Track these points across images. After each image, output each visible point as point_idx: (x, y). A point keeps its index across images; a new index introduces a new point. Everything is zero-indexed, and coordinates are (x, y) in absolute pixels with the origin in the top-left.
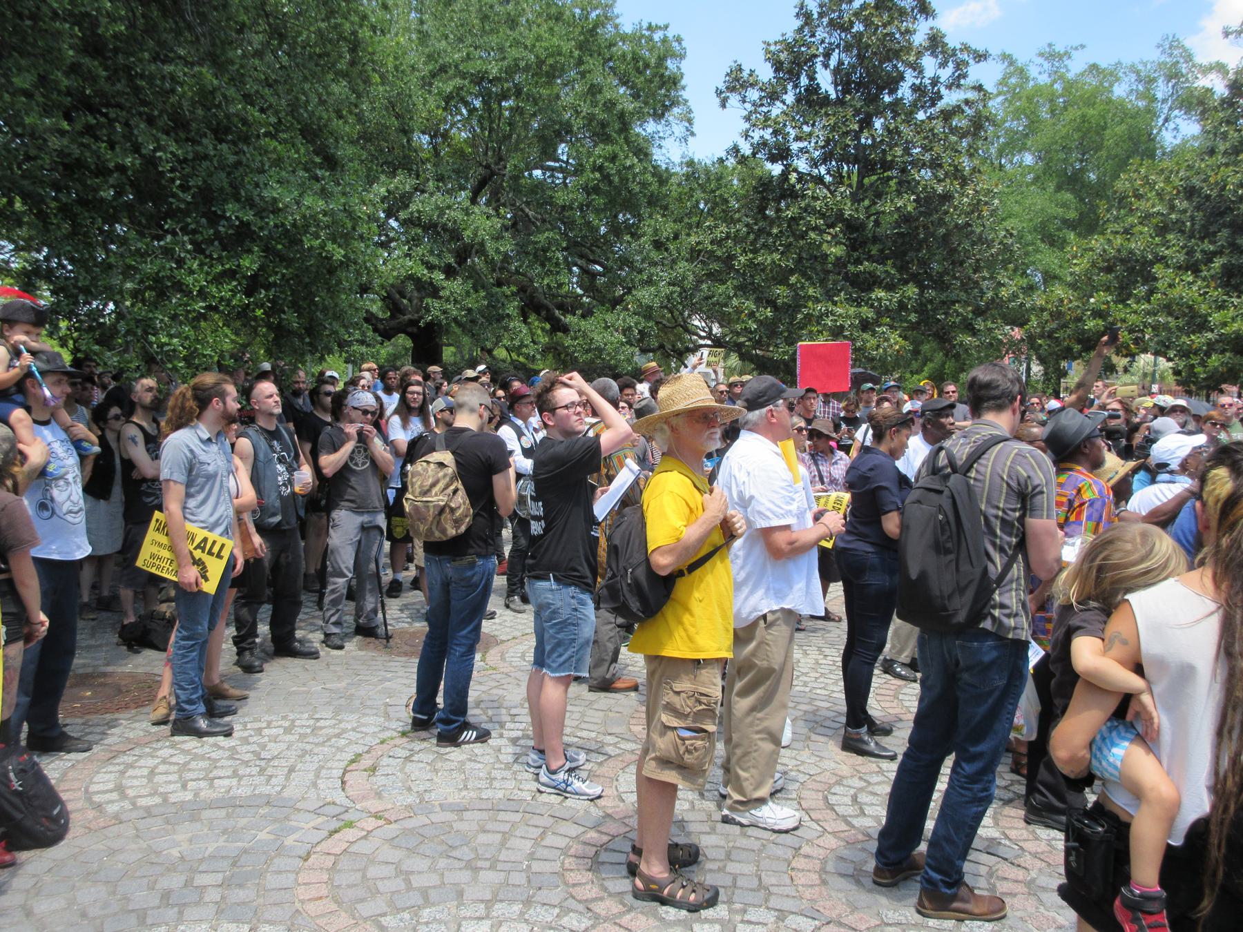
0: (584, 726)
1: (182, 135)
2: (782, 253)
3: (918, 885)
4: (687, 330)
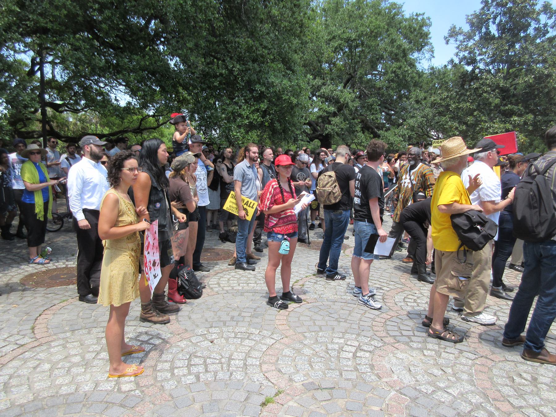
0: (382, 278)
1: (242, 62)
2: (471, 103)
3: (523, 348)
4: (429, 137)
